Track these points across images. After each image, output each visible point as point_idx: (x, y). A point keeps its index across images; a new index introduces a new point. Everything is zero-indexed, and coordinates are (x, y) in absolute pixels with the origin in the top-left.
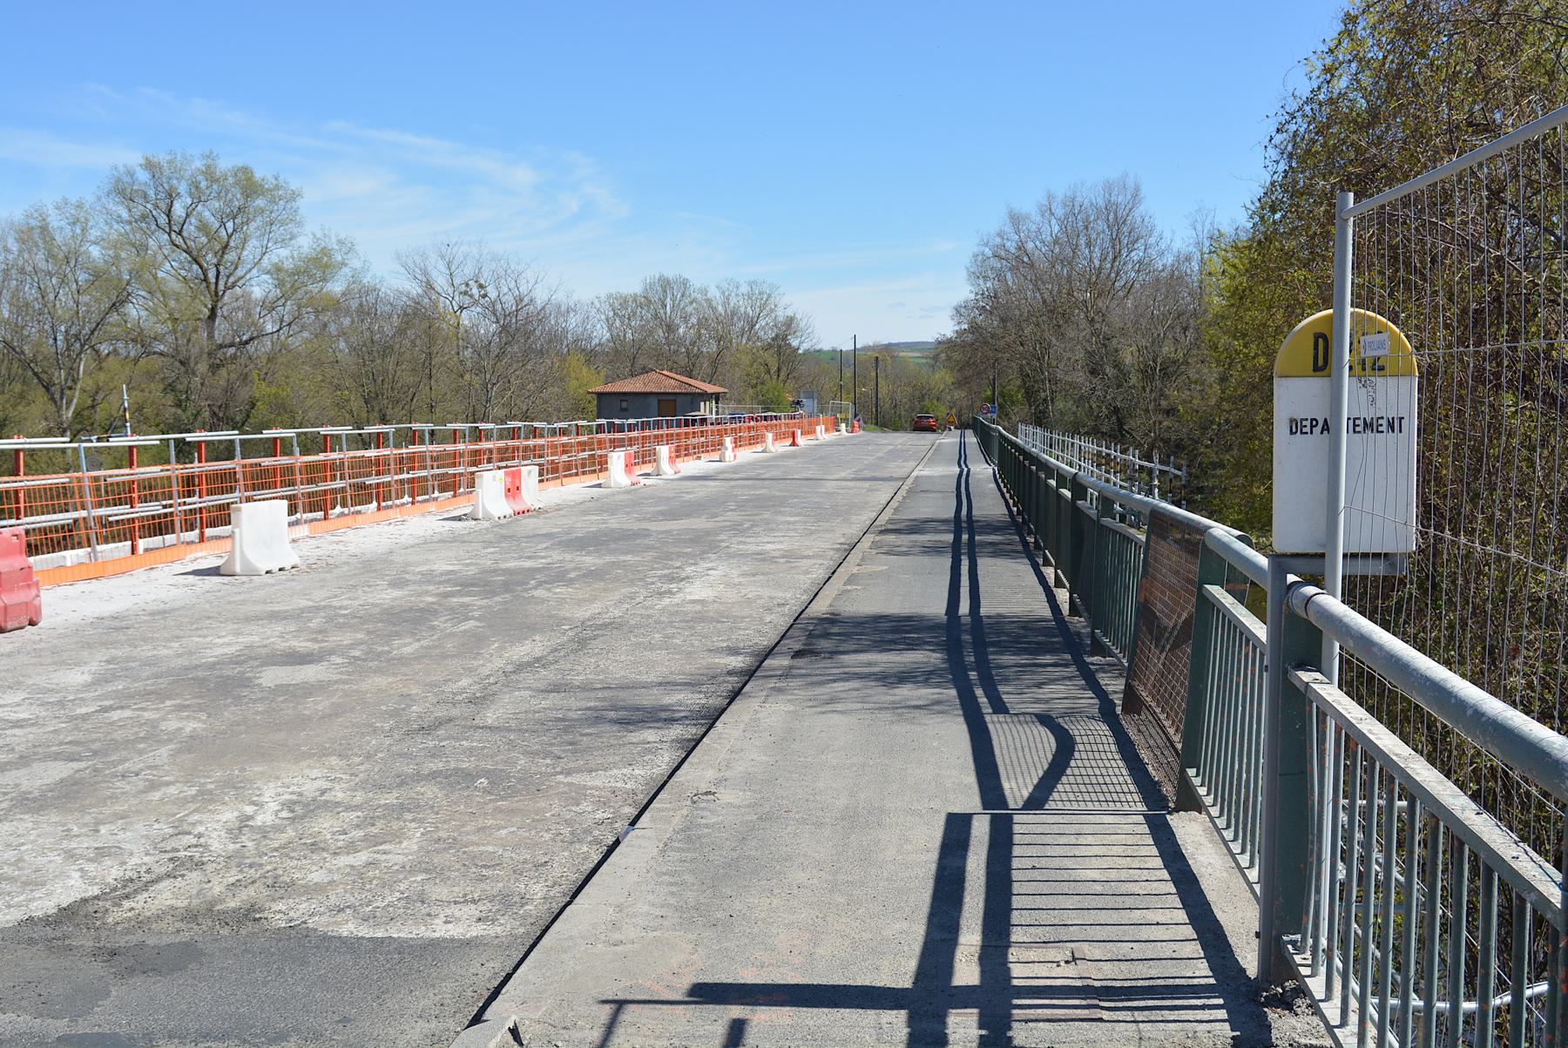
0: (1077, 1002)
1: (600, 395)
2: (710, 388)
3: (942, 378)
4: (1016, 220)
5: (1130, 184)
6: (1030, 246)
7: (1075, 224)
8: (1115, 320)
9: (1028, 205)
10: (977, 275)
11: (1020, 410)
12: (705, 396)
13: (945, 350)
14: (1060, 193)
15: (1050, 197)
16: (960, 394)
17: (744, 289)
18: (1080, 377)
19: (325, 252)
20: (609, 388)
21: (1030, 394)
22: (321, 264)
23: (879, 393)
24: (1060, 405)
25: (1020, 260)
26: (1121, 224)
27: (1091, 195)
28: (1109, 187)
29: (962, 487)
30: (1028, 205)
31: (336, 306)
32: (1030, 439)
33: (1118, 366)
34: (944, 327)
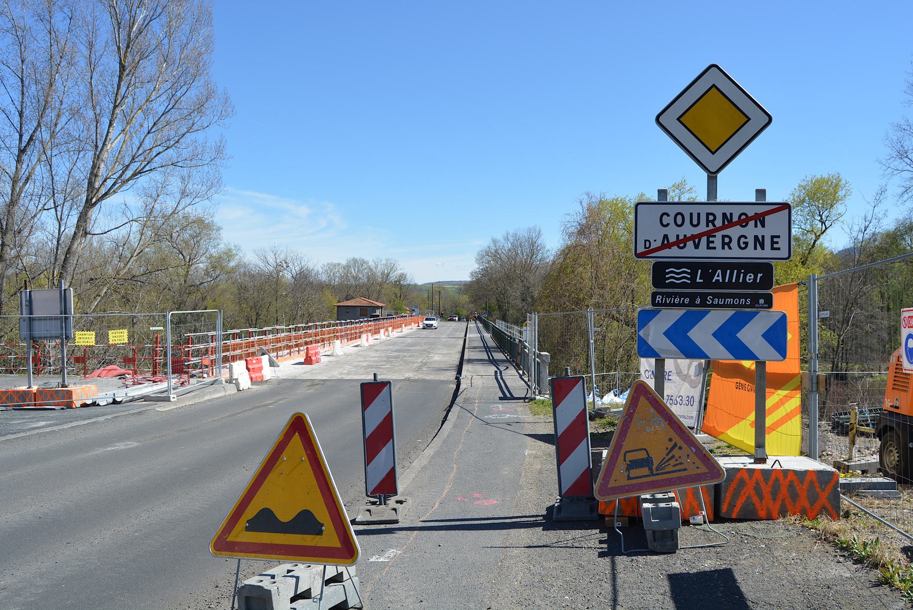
0: (523, 519)
1: (338, 306)
2: (380, 305)
3: (465, 298)
4: (495, 241)
5: (537, 229)
6: (500, 252)
7: (517, 244)
8: (531, 280)
9: (499, 236)
10: (480, 259)
11: (496, 313)
12: (378, 307)
13: (466, 287)
14: (511, 232)
15: (508, 234)
16: (471, 306)
17: (384, 262)
18: (518, 302)
19: (230, 250)
20: (341, 304)
21: (500, 307)
22: (229, 254)
23: (439, 304)
24: (511, 312)
25: (495, 255)
26: (533, 247)
27: (523, 233)
28: (529, 230)
29: (482, 338)
30: (499, 236)
31: (233, 270)
32: (500, 325)
33: (532, 297)
34: (467, 278)
